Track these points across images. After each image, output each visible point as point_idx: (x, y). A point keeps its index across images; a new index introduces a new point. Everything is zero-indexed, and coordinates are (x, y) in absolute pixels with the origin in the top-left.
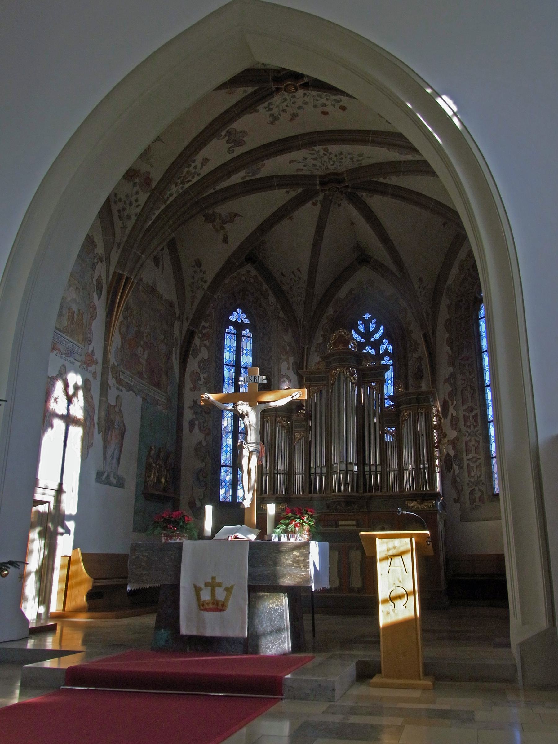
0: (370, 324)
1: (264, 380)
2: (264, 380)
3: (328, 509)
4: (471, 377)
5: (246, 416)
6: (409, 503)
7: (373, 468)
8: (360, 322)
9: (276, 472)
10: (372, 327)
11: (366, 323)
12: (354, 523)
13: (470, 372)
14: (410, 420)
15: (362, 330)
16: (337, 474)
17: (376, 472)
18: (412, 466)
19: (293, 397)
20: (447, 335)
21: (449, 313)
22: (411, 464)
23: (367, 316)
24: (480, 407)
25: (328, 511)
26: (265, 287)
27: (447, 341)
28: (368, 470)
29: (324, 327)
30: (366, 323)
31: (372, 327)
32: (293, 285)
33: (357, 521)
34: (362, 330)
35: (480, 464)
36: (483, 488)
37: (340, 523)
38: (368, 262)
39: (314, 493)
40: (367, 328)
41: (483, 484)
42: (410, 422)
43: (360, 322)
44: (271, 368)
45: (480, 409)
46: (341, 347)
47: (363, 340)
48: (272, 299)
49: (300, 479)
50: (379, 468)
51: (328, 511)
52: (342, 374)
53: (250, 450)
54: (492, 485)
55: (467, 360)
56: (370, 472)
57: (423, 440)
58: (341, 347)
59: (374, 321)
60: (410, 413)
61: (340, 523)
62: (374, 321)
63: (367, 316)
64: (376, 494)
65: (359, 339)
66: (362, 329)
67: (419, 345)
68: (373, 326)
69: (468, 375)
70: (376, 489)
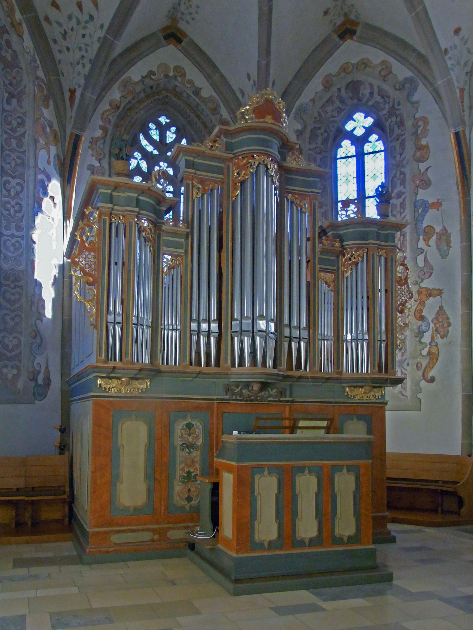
0: (168, 132)
3: (227, 394)
6: (351, 391)
8: (152, 126)
9: (111, 318)
10: (170, 137)
11: (163, 130)
12: (324, 423)
22: (351, 334)
26: (18, 16)
29: (105, 116)
30: (163, 130)
31: (170, 137)
32: (72, 29)
33: (331, 421)
37: (302, 423)
38: (179, 41)
40: (163, 136)
44: (24, 152)
46: (269, 119)
47: (156, 152)
48: (28, 43)
49: (172, 338)
50: (305, 334)
51: (227, 397)
58: (269, 119)
59: (173, 129)
61: (302, 423)
62: (173, 129)
63: (163, 120)
64: (208, 370)
65: (150, 148)
66: (155, 134)
70: (208, 363)
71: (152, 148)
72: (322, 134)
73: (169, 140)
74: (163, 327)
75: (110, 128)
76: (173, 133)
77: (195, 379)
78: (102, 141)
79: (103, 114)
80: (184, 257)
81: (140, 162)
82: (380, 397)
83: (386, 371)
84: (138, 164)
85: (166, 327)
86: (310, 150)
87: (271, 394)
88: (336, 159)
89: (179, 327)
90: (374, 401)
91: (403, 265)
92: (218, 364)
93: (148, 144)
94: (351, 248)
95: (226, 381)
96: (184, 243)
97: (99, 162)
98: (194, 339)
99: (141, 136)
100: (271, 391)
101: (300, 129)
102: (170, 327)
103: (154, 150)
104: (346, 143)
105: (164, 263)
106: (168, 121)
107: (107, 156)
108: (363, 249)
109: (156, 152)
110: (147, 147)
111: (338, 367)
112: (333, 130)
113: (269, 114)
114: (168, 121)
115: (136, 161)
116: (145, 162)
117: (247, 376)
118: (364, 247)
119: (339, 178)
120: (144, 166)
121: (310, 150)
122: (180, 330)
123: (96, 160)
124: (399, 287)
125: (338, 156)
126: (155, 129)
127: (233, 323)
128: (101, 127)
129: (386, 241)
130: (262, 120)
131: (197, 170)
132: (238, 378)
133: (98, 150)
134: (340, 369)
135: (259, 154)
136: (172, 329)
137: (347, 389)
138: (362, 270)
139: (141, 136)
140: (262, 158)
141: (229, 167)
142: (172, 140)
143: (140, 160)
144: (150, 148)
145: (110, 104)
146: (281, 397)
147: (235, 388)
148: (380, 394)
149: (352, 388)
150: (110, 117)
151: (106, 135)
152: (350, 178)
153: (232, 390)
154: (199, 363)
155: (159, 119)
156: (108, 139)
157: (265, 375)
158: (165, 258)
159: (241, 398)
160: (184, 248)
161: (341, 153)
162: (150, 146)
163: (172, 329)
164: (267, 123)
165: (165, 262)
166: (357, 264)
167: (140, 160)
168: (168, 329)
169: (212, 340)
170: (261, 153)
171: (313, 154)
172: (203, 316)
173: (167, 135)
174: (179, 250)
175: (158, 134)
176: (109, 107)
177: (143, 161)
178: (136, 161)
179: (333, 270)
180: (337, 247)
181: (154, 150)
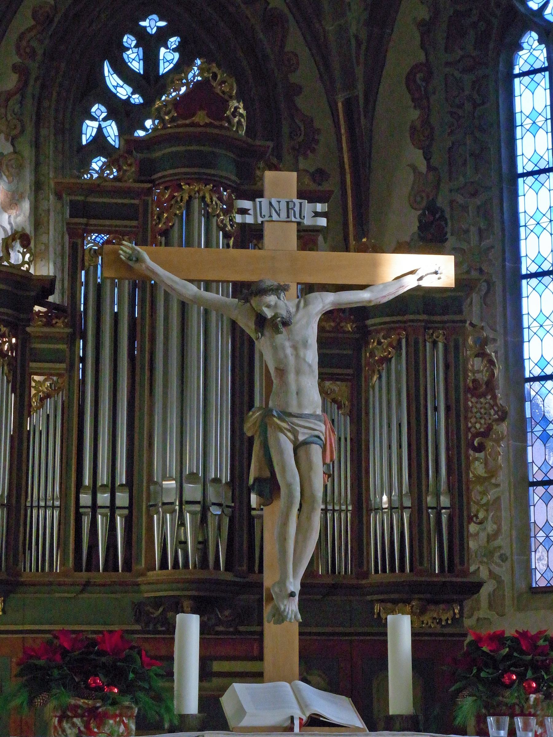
0: (163, 50)
1: (317, 214)
2: (317, 214)
4: (486, 243)
5: (283, 329)
7: (103, 498)
8: (129, 40)
10: (168, 58)
11: (150, 45)
13: (480, 231)
14: (398, 362)
15: (137, 66)
16: (173, 512)
17: (113, 507)
18: (390, 500)
19: (420, 279)
20: (415, 114)
21: (423, 46)
23: (152, 24)
24: (506, 334)
25: (138, 627)
27: (413, 129)
28: (89, 503)
29: (24, 43)
30: (150, 45)
31: (168, 58)
34: (137, 66)
35: (498, 498)
36: (502, 570)
39: (88, 570)
40: (151, 60)
41: (503, 558)
42: (400, 366)
43: (129, 40)
45: (506, 342)
46: (201, 117)
47: (137, 99)
51: (138, 627)
52: (196, 203)
53: (301, 438)
54: (529, 561)
55: (474, 194)
56: (94, 507)
57: (438, 422)
58: (201, 117)
59: (174, 41)
60: (399, 342)
62: (174, 41)
65: (123, 91)
66: (134, 60)
67: (318, 131)
68: (169, 56)
69: (474, 238)
71: (129, 90)
72: (474, 25)
73: (164, 68)
74: (28, 504)
75: (33, 66)
76: (174, 50)
77: (81, 596)
78: (18, 97)
79: (21, 37)
80: (66, 376)
81: (104, 124)
82: (449, 622)
83: (451, 570)
84: (100, 129)
85: (35, 504)
86: (447, 64)
87: (220, 620)
88: (510, 77)
89: (57, 503)
90: (438, 629)
91: (482, 354)
92: (128, 566)
93: (121, 83)
94: (378, 332)
95: (137, 598)
96: (68, 354)
97: (13, 145)
98: (86, 521)
99: (107, 68)
100: (221, 613)
101: (427, 18)
102: (42, 504)
103: (133, 93)
104: (531, 39)
105: (32, 389)
106: (162, 24)
107: (30, 128)
108: (399, 331)
109: (137, 99)
110: (118, 89)
111: (360, 565)
112: (498, 12)
113: (201, 108)
114: (162, 24)
115: (95, 124)
116: (114, 124)
117: (164, 586)
118: (400, 328)
119: (518, 119)
120: (112, 131)
121: (447, 64)
122: (60, 507)
123: (7, 140)
124: (474, 400)
125: (516, 71)
126: (135, 47)
127: (152, 487)
128: (15, 68)
129: (444, 314)
130: (187, 122)
131: (89, 218)
132: (158, 591)
133: (9, 118)
134: (365, 568)
135: (189, 181)
136: (46, 507)
137: (377, 607)
138: (398, 373)
139: (107, 68)
140: (196, 187)
141: (146, 204)
142: (172, 66)
143: (105, 120)
144: (123, 91)
145: (34, 16)
146: (242, 623)
147: (151, 610)
148: (450, 614)
149: (389, 605)
150: (34, 44)
151: (26, 84)
152: (540, 121)
153: (148, 613)
154: (92, 565)
155: (142, 24)
156: (33, 88)
157: (173, 582)
158: (35, 381)
159: (164, 629)
160: (68, 360)
161: (522, 62)
162: (125, 86)
163: (46, 507)
164: (197, 125)
165: (33, 387)
166: (388, 360)
167: (105, 120)
168: (39, 507)
169: (119, 522)
170: (192, 179)
171: (457, 74)
172: (103, 478)
173: (161, 57)
174: (58, 366)
175: (141, 57)
176: (33, 23)
177: (109, 122)
178: (95, 124)
179: (348, 375)
180: (349, 332)
181: (133, 93)
